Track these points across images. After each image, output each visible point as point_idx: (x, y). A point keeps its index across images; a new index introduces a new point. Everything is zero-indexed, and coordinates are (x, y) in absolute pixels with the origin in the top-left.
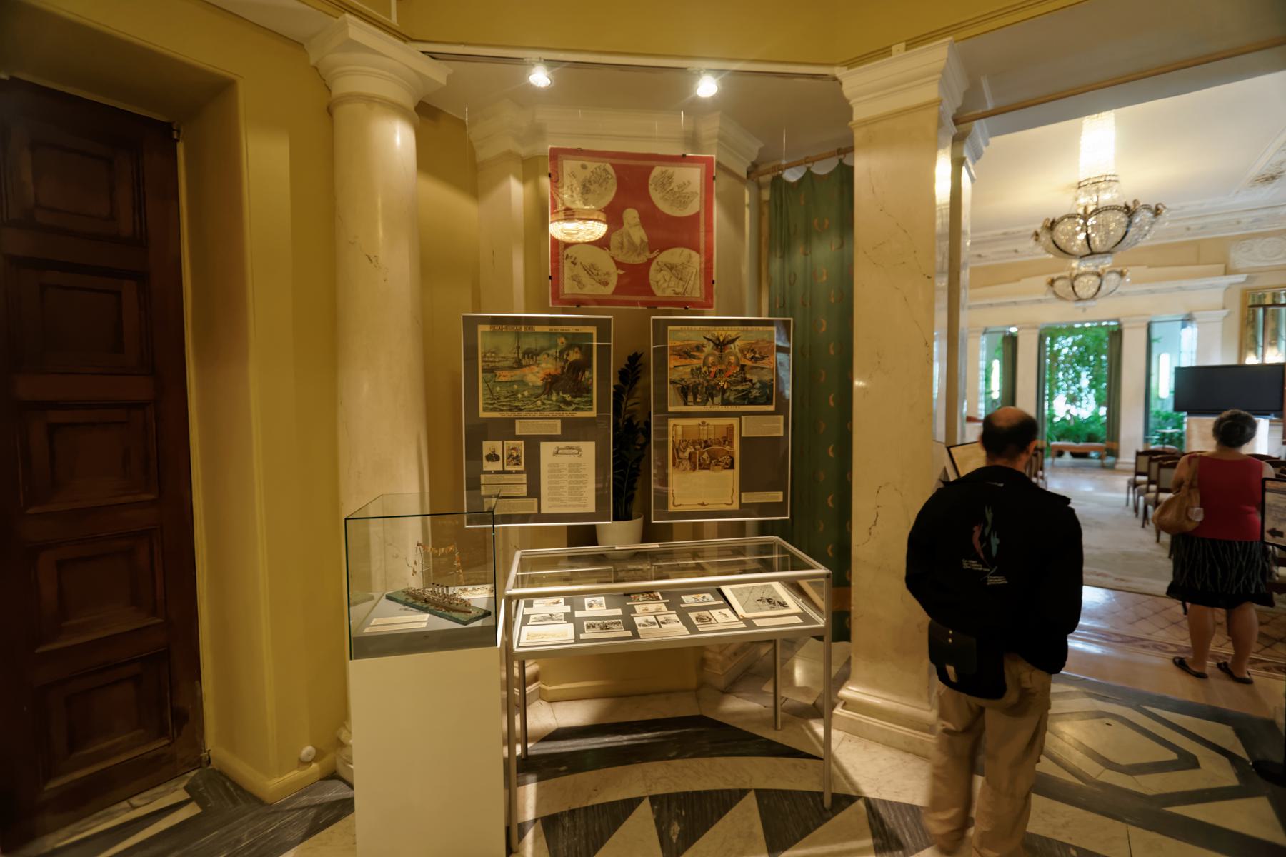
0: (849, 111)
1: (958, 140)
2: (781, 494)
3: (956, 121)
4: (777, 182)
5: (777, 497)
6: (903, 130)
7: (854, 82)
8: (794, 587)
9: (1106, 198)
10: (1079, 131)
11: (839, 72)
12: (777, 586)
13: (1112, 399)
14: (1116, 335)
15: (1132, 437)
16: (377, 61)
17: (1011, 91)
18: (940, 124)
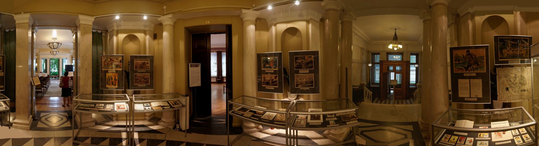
0: (15, 22)
1: (33, 29)
2: (285, 130)
3: (32, 26)
4: (5, 32)
5: (2, 87)
6: (22, 26)
7: (16, 17)
8: (5, 102)
9: (56, 41)
10: (52, 32)
11: (14, 15)
12: (2, 103)
13: (59, 69)
14: (59, 60)
15: (61, 75)
16: (249, 15)
17: (38, 24)
18: (29, 25)
